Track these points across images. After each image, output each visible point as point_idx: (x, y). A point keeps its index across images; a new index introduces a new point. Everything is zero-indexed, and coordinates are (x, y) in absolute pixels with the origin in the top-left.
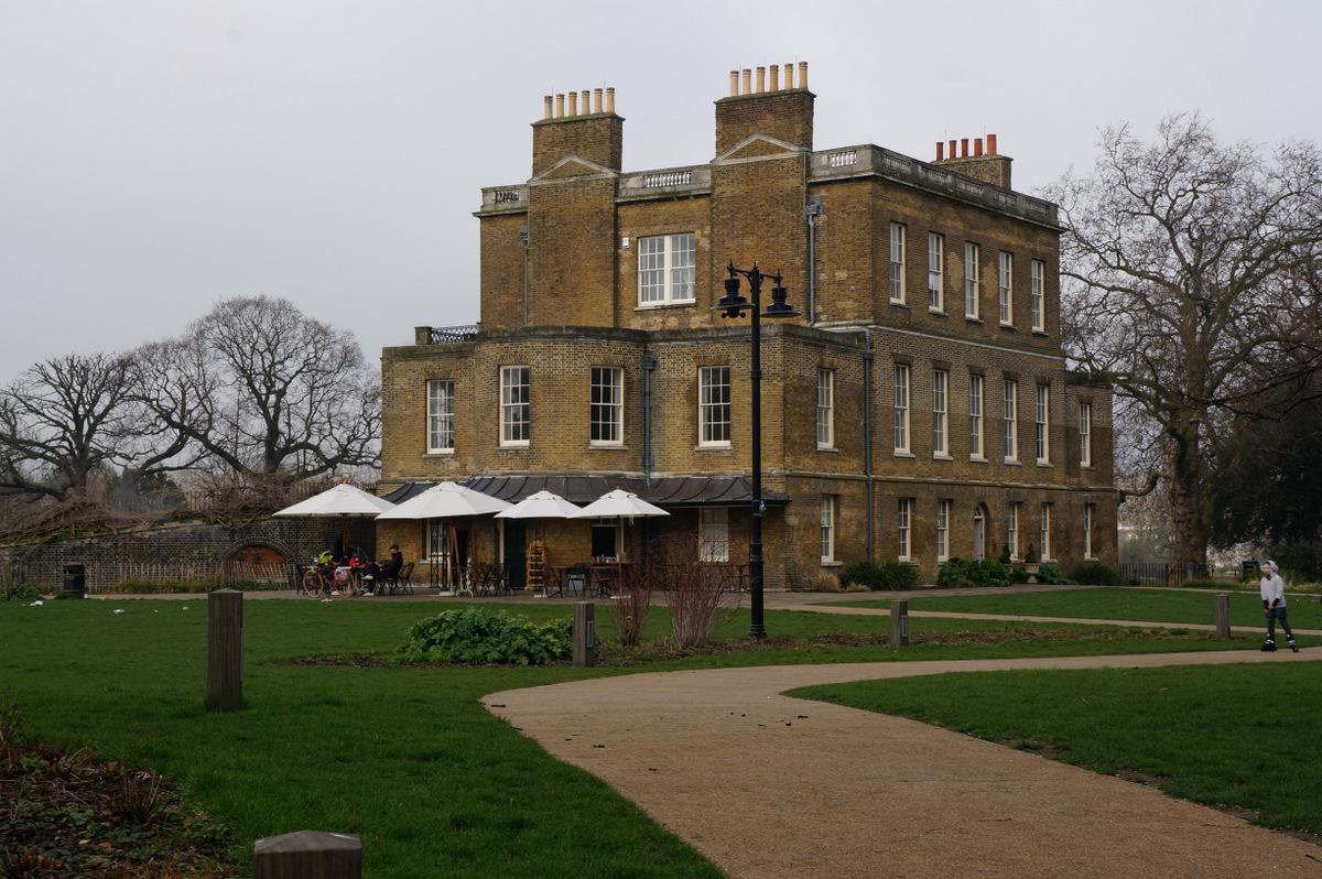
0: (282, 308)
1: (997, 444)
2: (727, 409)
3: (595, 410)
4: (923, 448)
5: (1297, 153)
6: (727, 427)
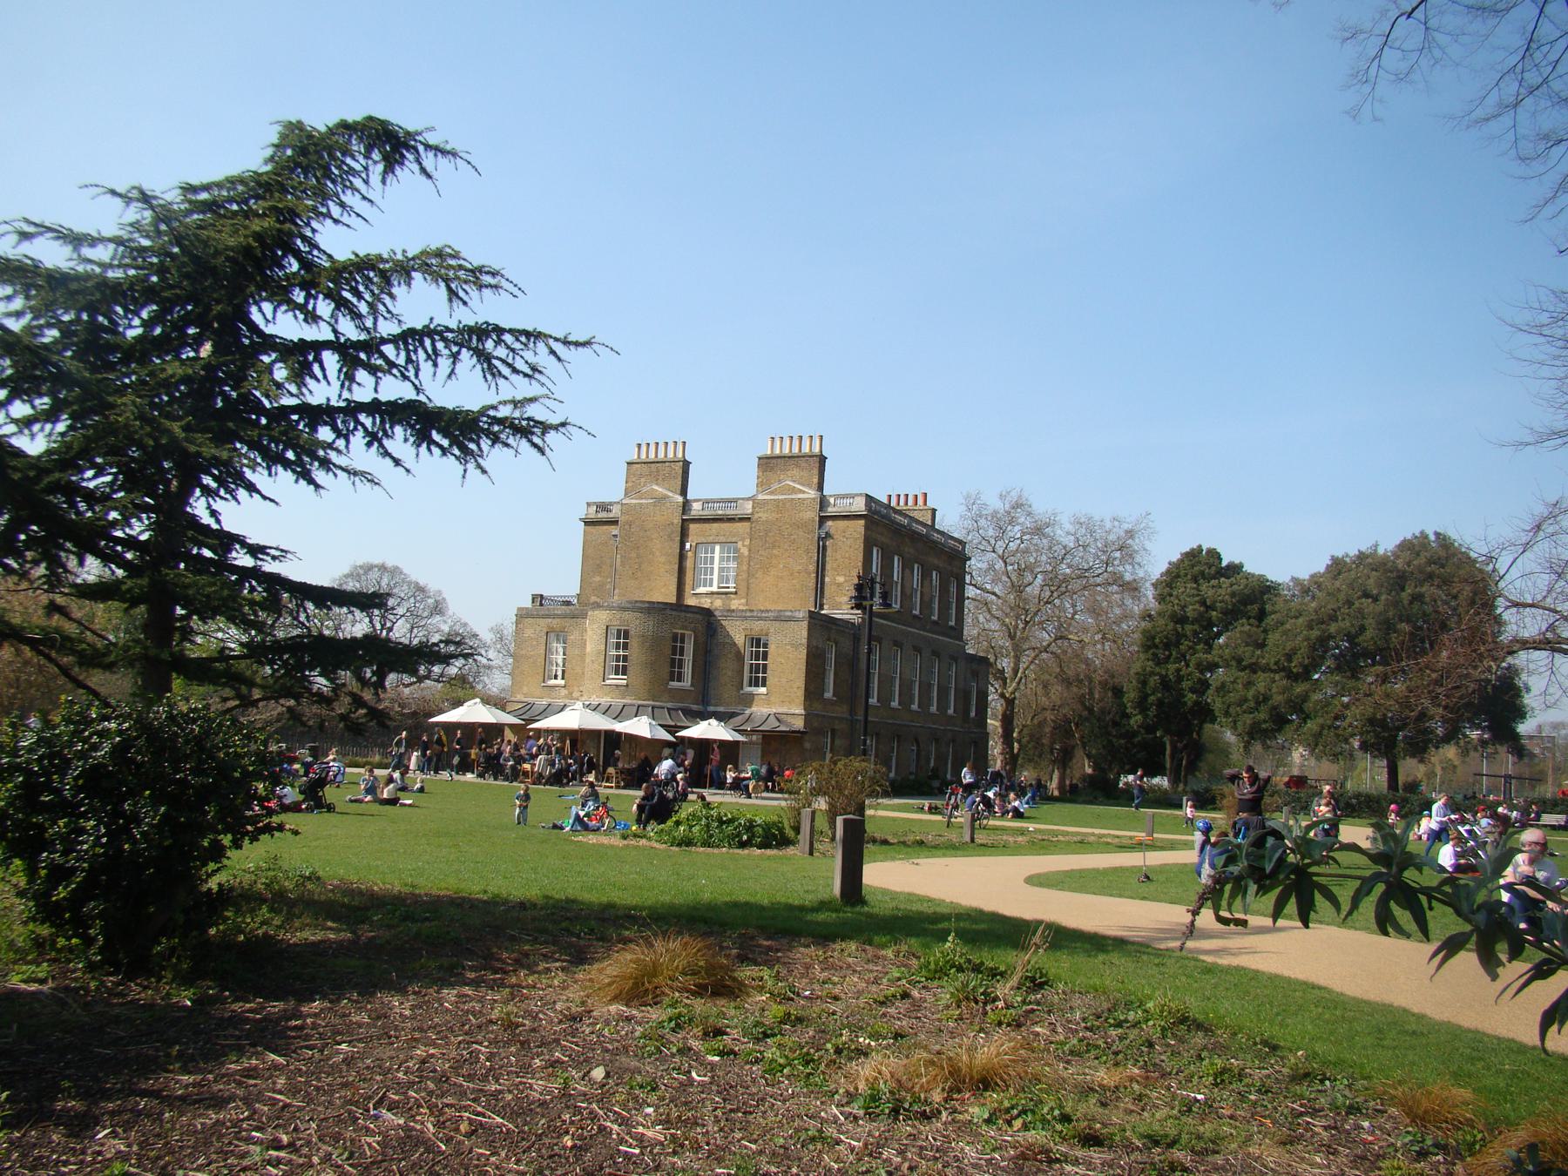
0: (395, 571)
1: (925, 701)
2: (765, 666)
3: (673, 661)
4: (885, 699)
5: (1082, 520)
6: (764, 679)
